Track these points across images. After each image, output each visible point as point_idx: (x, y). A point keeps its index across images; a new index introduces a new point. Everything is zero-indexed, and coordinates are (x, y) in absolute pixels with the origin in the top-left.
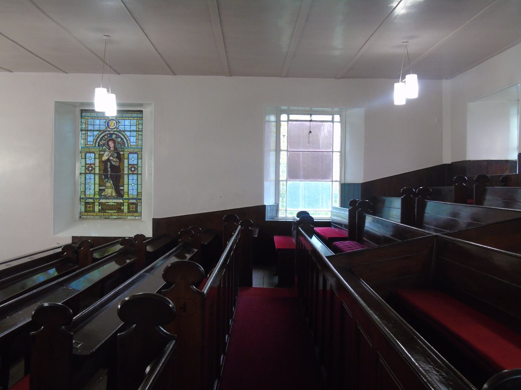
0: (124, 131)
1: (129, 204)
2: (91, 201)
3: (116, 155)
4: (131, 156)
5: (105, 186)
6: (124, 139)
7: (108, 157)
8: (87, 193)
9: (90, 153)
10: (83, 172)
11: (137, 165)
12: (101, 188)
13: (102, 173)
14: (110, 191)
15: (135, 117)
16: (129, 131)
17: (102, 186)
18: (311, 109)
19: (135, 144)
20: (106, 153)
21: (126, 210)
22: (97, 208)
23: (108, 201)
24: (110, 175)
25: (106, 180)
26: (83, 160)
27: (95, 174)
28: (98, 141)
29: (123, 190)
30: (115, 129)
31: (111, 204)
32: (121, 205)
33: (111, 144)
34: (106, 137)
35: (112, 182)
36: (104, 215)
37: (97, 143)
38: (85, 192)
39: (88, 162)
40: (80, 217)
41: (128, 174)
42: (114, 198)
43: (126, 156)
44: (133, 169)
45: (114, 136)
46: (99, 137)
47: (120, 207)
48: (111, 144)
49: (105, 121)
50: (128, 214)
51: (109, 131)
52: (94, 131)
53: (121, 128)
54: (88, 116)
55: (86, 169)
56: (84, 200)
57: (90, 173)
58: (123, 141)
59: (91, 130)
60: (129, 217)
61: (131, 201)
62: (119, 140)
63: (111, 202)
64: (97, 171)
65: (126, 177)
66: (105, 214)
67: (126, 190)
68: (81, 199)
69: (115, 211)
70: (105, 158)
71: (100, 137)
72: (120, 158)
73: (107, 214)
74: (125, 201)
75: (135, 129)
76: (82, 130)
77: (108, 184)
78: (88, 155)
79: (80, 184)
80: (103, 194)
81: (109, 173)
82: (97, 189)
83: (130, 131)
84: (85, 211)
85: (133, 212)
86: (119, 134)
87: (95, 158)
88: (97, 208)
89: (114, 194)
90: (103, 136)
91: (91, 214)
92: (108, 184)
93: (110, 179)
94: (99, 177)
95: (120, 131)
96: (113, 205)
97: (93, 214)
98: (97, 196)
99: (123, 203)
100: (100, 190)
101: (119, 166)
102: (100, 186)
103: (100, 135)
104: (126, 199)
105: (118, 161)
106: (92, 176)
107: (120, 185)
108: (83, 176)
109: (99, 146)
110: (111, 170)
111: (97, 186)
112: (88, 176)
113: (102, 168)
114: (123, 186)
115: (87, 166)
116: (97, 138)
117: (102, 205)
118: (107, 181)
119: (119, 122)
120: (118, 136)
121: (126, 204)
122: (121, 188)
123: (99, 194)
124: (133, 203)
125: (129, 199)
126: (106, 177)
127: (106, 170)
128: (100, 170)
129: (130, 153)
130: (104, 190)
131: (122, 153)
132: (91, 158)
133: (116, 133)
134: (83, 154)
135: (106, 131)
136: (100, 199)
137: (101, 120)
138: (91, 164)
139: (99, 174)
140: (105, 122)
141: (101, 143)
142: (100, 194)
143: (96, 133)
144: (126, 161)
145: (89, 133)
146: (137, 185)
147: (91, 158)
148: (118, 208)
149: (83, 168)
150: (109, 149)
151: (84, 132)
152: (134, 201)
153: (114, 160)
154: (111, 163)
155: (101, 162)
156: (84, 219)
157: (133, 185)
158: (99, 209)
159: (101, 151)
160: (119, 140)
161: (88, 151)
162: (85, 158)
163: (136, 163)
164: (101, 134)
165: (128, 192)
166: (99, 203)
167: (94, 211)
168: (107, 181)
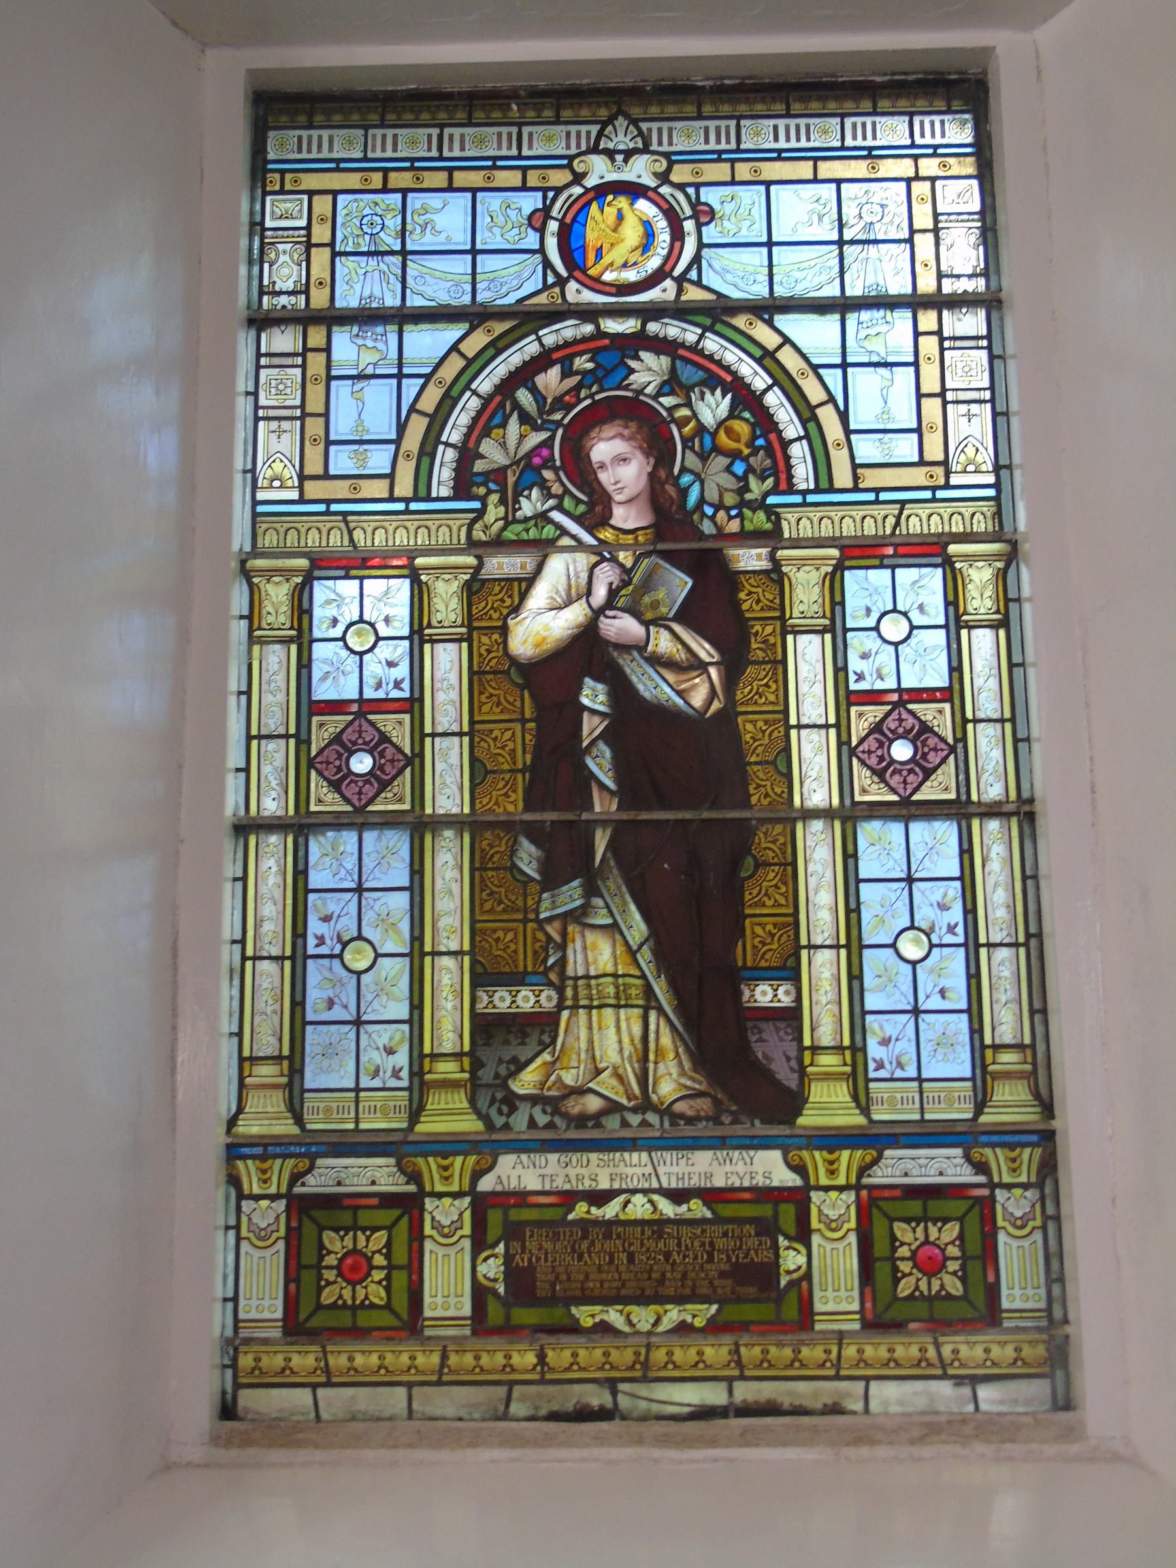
0: (768, 308)
1: (873, 1205)
2: (378, 1175)
3: (678, 585)
4: (865, 588)
5: (558, 978)
6: (774, 399)
7: (576, 615)
8: (327, 1071)
9: (356, 564)
10: (271, 806)
11: (950, 694)
12: (502, 1000)
13: (513, 806)
14: (613, 1043)
15: (894, 152)
16: (820, 307)
17: (516, 979)
18: (644, 325)
19: (905, 447)
20: (560, 569)
21: (838, 1294)
22: (449, 1280)
23: (595, 1171)
24: (620, 830)
25: (571, 895)
26: (276, 661)
27: (420, 827)
28: (453, 434)
29: (790, 1017)
30: (665, 292)
31: (639, 1208)
32: (768, 1229)
33: (618, 461)
34: (550, 380)
35: (637, 928)
36: (544, 1374)
37: (446, 458)
38: (293, 1062)
39: (336, 678)
40: (228, 1411)
41: (849, 815)
42: (678, 1132)
43: (806, 591)
44: (902, 751)
45: (648, 371)
46: (427, 451)
47: (754, 1248)
48: (618, 461)
49: (530, 202)
50: (876, 1350)
51: (589, 314)
52: (404, 317)
53: (735, 275)
54: (338, 167)
55: (306, 763)
56: (280, 1172)
57: (359, 820)
58: (765, 422)
59: (366, 317)
60: (889, 1396)
61: (901, 1167)
62: (713, 408)
63: (640, 1183)
64: (448, 792)
65: (817, 849)
66: (559, 1357)
67: (825, 1022)
68: (234, 1151)
69: (701, 1314)
70: (543, 624)
71: (485, 384)
72: (731, 617)
73: (590, 1354)
74: (430, 1167)
75: (899, 286)
76: (260, 322)
77: (596, 954)
78: (335, 599)
79: (229, 955)
80: (526, 1082)
81: (602, 805)
82: (449, 1028)
83: (842, 306)
84: (295, 1327)
85: (940, 1317)
86: (712, 344)
87: (420, 635)
88: (449, 1280)
89: (669, 1083)
90: (524, 375)
91: (367, 1358)
92: (596, 954)
93: (614, 883)
94: (479, 867)
95: (718, 313)
96: (659, 1225)
97: (399, 1357)
98: (451, 1115)
99: (799, 1198)
100: (487, 1028)
101: (728, 716)
102: (483, 977)
103: (475, 365)
104: (832, 1140)
105: (704, 650)
106: (388, 856)
107: (744, 954)
108: (271, 858)
109: (463, 486)
110: (620, 767)
111: (448, 977)
112: (331, 859)
113: (516, 743)
114: (789, 971)
115: (323, 730)
116: (449, 402)
117: (513, 1232)
118: (578, 916)
119: (704, 214)
120: (696, 372)
121: (833, 1207)
122: (764, 995)
123: (474, 1087)
124: (926, 1197)
125: (876, 1139)
126: (567, 857)
127: (554, 769)
128: (480, 772)
129: (860, 552)
130: (542, 1026)
131: (750, 559)
132: (365, 633)
133: (672, 330)
134: (277, 594)
135: (553, 316)
136: (486, 1149)
137: (491, 202)
138: (367, 707)
139: (472, 825)
140: (538, 221)
141: (492, 454)
142: (488, 1087)
143: (426, 344)
144: (808, 656)
145: (346, 347)
146: (972, 946)
147: (365, 633)
148: (734, 1269)
149: (276, 758)
150: (597, 510)
151: (283, 340)
152: (945, 1166)
153: (663, 643)
154: (622, 691)
155: (492, 671)
156: (283, 1433)
157: (911, 948)
158: (480, 1293)
159: (498, 544)
160: (713, 408)
161: (336, 540)
162: (301, 637)
163: (937, 678)
164: (497, 347)
165: (858, 1049)
166: (482, 1204)
167: (412, 1322)
168: (578, 916)
